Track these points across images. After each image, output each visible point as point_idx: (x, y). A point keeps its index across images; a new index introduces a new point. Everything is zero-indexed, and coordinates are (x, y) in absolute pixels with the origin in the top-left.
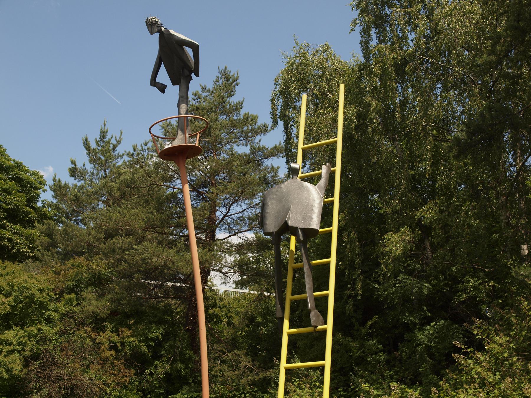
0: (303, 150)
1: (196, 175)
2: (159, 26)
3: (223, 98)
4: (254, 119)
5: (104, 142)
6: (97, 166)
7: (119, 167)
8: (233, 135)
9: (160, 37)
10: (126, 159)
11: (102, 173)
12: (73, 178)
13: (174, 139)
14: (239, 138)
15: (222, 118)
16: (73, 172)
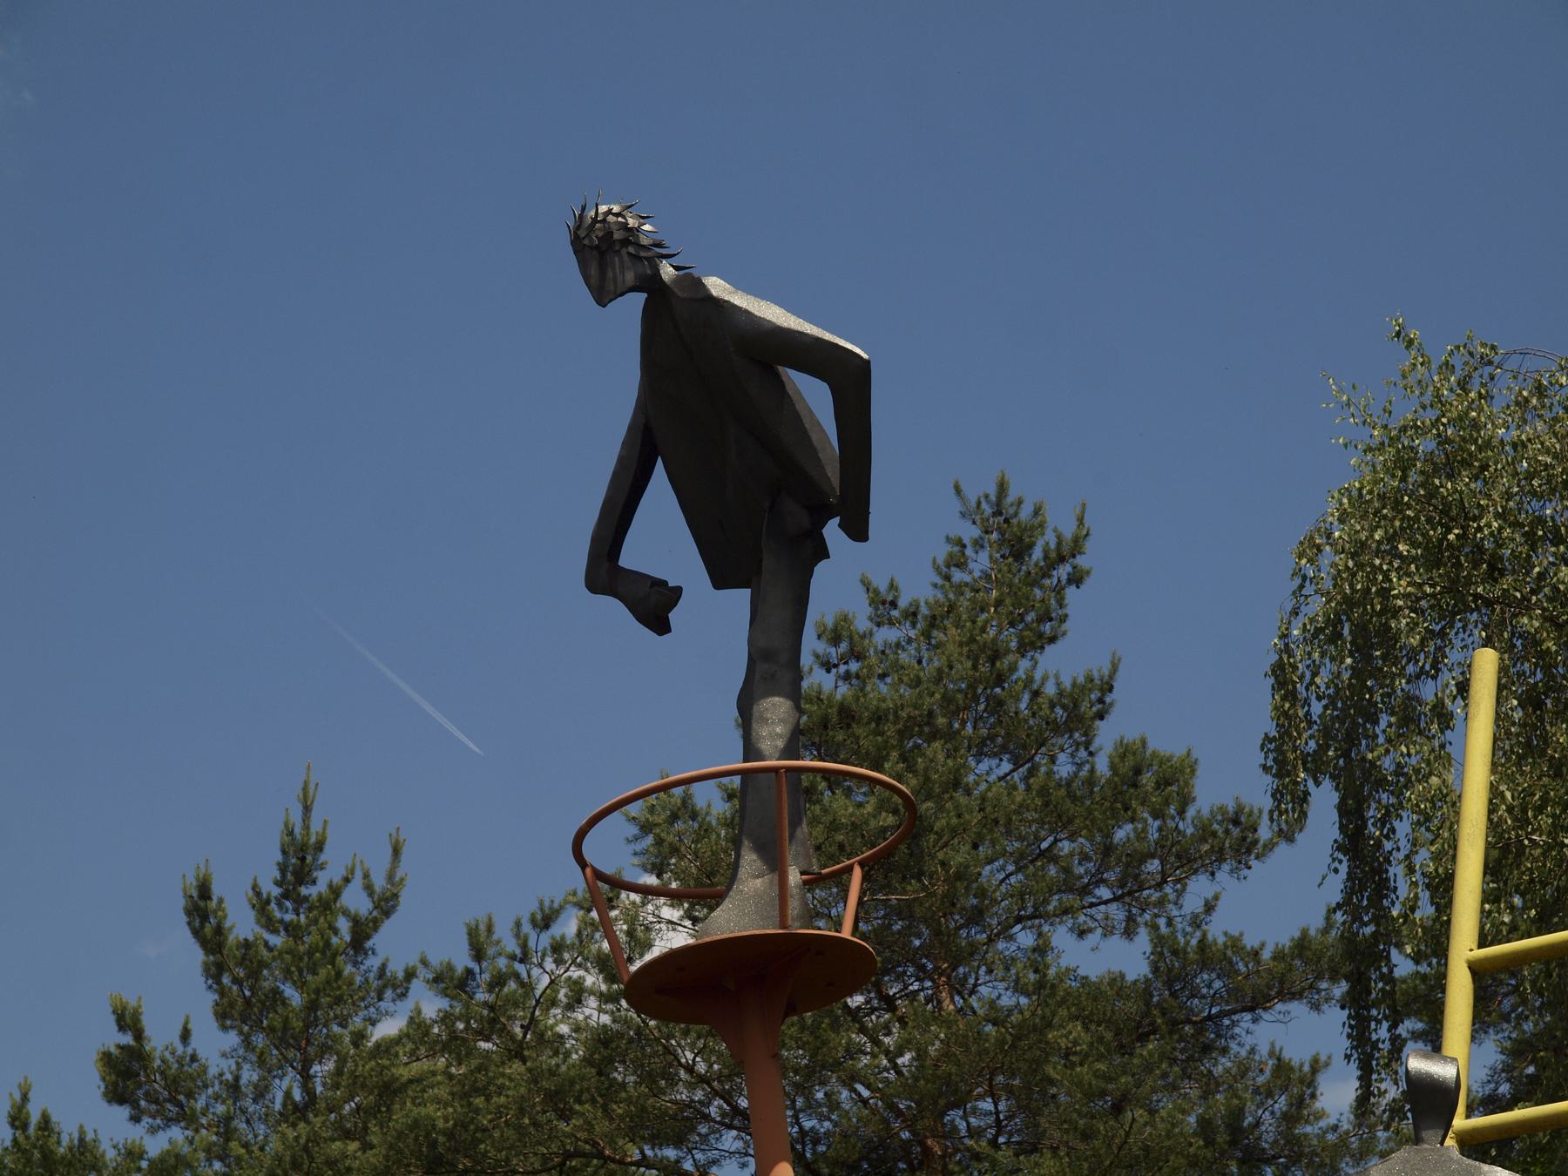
0: (1478, 970)
1: (833, 1103)
2: (646, 256)
3: (994, 658)
4: (1174, 780)
5: (300, 901)
6: (259, 1040)
7: (386, 1048)
8: (1052, 871)
9: (649, 313)
10: (432, 1006)
11: (287, 1085)
12: (124, 1112)
13: (713, 899)
14: (1085, 891)
15: (989, 771)
16: (127, 1075)
